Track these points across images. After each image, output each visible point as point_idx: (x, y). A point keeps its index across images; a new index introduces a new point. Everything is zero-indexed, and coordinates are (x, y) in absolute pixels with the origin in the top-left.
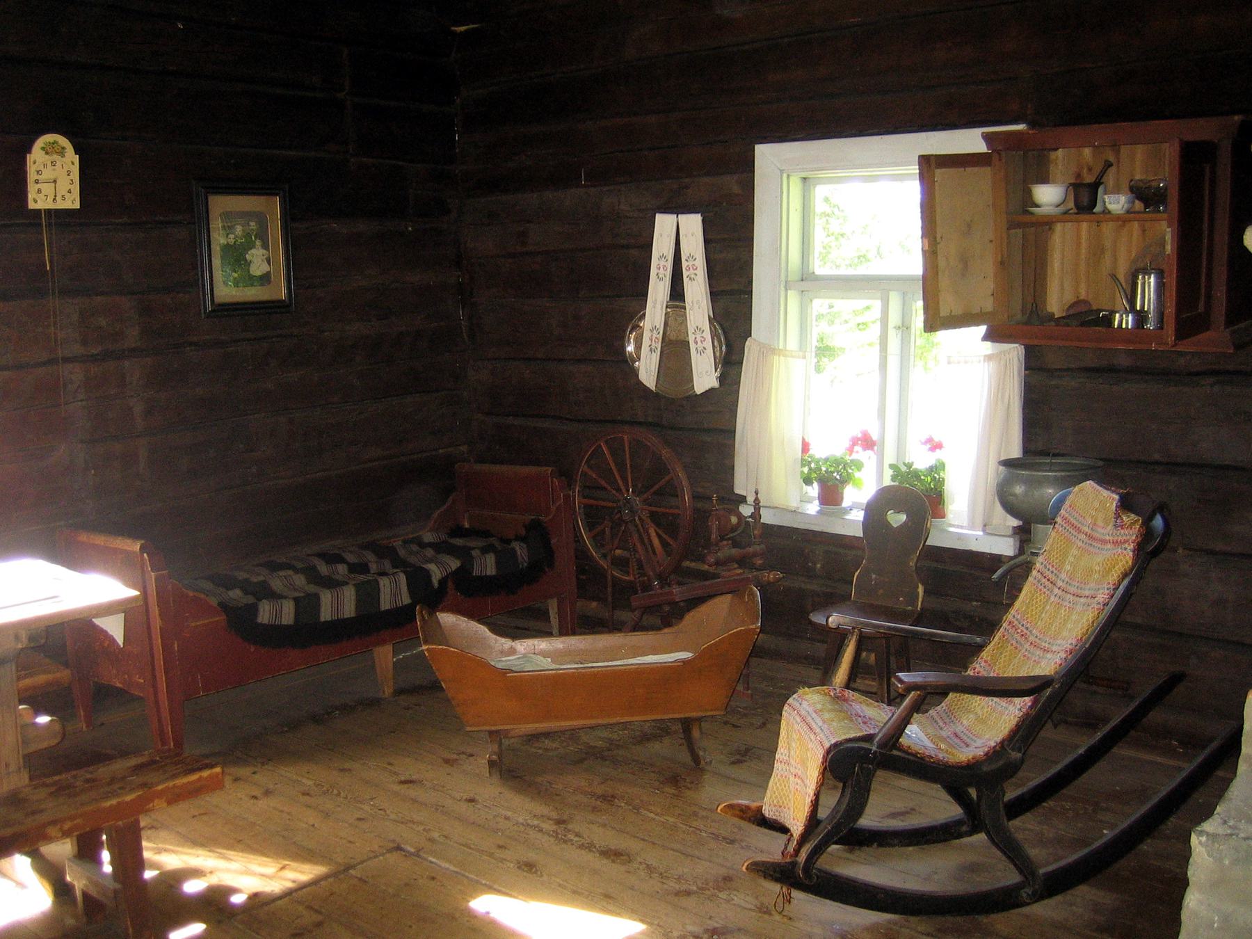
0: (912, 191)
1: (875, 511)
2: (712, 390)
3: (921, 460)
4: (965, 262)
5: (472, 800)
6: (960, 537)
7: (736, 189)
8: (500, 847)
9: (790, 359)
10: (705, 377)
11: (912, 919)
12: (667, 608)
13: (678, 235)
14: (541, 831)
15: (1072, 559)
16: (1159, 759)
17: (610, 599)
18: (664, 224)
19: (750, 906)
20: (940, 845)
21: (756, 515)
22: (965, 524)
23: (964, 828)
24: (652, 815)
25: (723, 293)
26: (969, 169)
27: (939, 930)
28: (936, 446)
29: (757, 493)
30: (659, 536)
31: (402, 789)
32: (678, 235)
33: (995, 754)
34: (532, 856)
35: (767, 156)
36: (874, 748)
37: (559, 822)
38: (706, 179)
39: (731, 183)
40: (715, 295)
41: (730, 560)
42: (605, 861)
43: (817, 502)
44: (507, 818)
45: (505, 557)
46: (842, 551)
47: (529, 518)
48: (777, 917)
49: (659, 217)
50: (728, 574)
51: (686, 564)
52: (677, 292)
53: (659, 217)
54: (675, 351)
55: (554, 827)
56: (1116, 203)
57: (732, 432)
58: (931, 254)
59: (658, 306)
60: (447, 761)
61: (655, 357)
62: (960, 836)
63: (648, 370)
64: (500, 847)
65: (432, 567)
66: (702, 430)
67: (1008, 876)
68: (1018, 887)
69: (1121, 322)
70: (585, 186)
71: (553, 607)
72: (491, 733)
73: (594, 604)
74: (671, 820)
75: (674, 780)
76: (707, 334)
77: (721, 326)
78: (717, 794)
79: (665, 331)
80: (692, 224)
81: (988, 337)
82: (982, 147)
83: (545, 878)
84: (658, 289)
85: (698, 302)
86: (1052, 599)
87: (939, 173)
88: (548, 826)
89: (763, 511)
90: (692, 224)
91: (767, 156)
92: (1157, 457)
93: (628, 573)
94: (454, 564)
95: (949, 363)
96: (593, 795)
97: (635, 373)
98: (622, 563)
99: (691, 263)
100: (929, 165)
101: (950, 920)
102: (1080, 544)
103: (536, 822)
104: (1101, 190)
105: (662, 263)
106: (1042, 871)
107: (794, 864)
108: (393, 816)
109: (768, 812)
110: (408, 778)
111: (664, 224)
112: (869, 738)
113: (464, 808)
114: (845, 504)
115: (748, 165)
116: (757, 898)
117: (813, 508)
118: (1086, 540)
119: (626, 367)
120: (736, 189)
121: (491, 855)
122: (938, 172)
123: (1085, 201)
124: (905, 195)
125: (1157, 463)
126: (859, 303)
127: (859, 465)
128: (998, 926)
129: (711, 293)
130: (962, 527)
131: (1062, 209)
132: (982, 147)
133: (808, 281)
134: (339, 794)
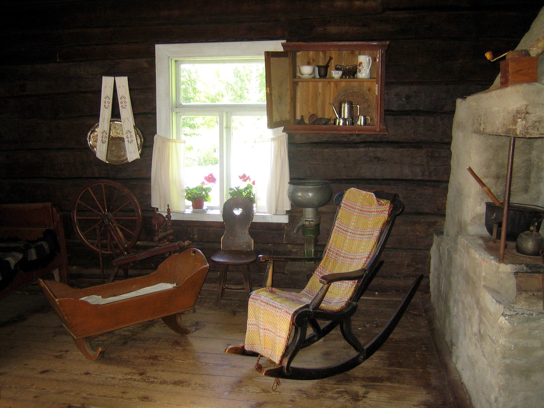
0: (261, 67)
1: (227, 209)
2: (137, 160)
3: (238, 184)
4: (280, 98)
5: (87, 374)
6: (264, 217)
7: (145, 65)
8: (124, 393)
9: (178, 144)
10: (132, 153)
11: (325, 379)
12: (132, 264)
13: (115, 87)
14: (135, 380)
15: (354, 220)
16: (368, 298)
17: (101, 264)
18: (107, 82)
19: (260, 391)
20: (308, 347)
21: (169, 216)
22: (266, 211)
23: (315, 339)
24: (181, 361)
25: (140, 114)
26: (282, 58)
27: (338, 381)
28: (244, 178)
29: (168, 206)
30: (121, 230)
31: (42, 376)
32: (115, 87)
33: (348, 304)
34: (142, 393)
35: (162, 51)
36: (311, 310)
37: (141, 374)
38: (129, 60)
39: (143, 62)
40: (136, 115)
41: (164, 238)
42: (178, 387)
43: (191, 208)
44: (113, 378)
45: (40, 250)
46: (207, 229)
47: (44, 229)
48: (274, 393)
49: (104, 78)
50: (164, 244)
51: (138, 243)
52: (116, 114)
53: (104, 78)
54: (115, 143)
55: (141, 377)
56: (336, 75)
57: (149, 179)
58: (269, 96)
59: (106, 121)
60: (57, 357)
61: (105, 146)
62: (314, 342)
63: (101, 152)
64: (124, 393)
65: (9, 259)
66: (136, 177)
67: (354, 353)
68: (358, 356)
69: (339, 123)
70: (59, 62)
71: (56, 273)
72: (86, 338)
73: (75, 267)
74: (191, 361)
75: (177, 343)
76: (133, 133)
77: (140, 130)
78: (209, 344)
79: (110, 134)
80: (123, 82)
81: (284, 131)
82: (281, 49)
83: (158, 402)
84: (105, 112)
85: (128, 118)
86: (348, 237)
87: (273, 60)
88: (136, 377)
89: (171, 214)
90: (123, 82)
91: (162, 51)
92: (344, 177)
93: (107, 251)
94: (20, 256)
95: (255, 142)
96: (146, 358)
97: (94, 154)
98: (104, 246)
99: (123, 100)
100: (269, 56)
101: (338, 376)
102: (356, 214)
103: (129, 377)
104: (329, 69)
105: (107, 100)
106: (365, 348)
107: (282, 367)
108: (52, 391)
109: (247, 348)
110: (43, 370)
111: (107, 82)
112: (307, 306)
113: (86, 378)
114: (205, 208)
115: (152, 55)
116: (258, 386)
117: (189, 211)
118: (359, 212)
119: (90, 151)
120: (145, 65)
121: (122, 398)
122: (272, 59)
123: (322, 73)
124: (258, 68)
125: (345, 180)
126: (208, 118)
127: (209, 189)
128: (356, 374)
129: (134, 114)
130: (265, 213)
131: (311, 76)
132: (281, 49)
133: (178, 108)
134: (10, 387)
